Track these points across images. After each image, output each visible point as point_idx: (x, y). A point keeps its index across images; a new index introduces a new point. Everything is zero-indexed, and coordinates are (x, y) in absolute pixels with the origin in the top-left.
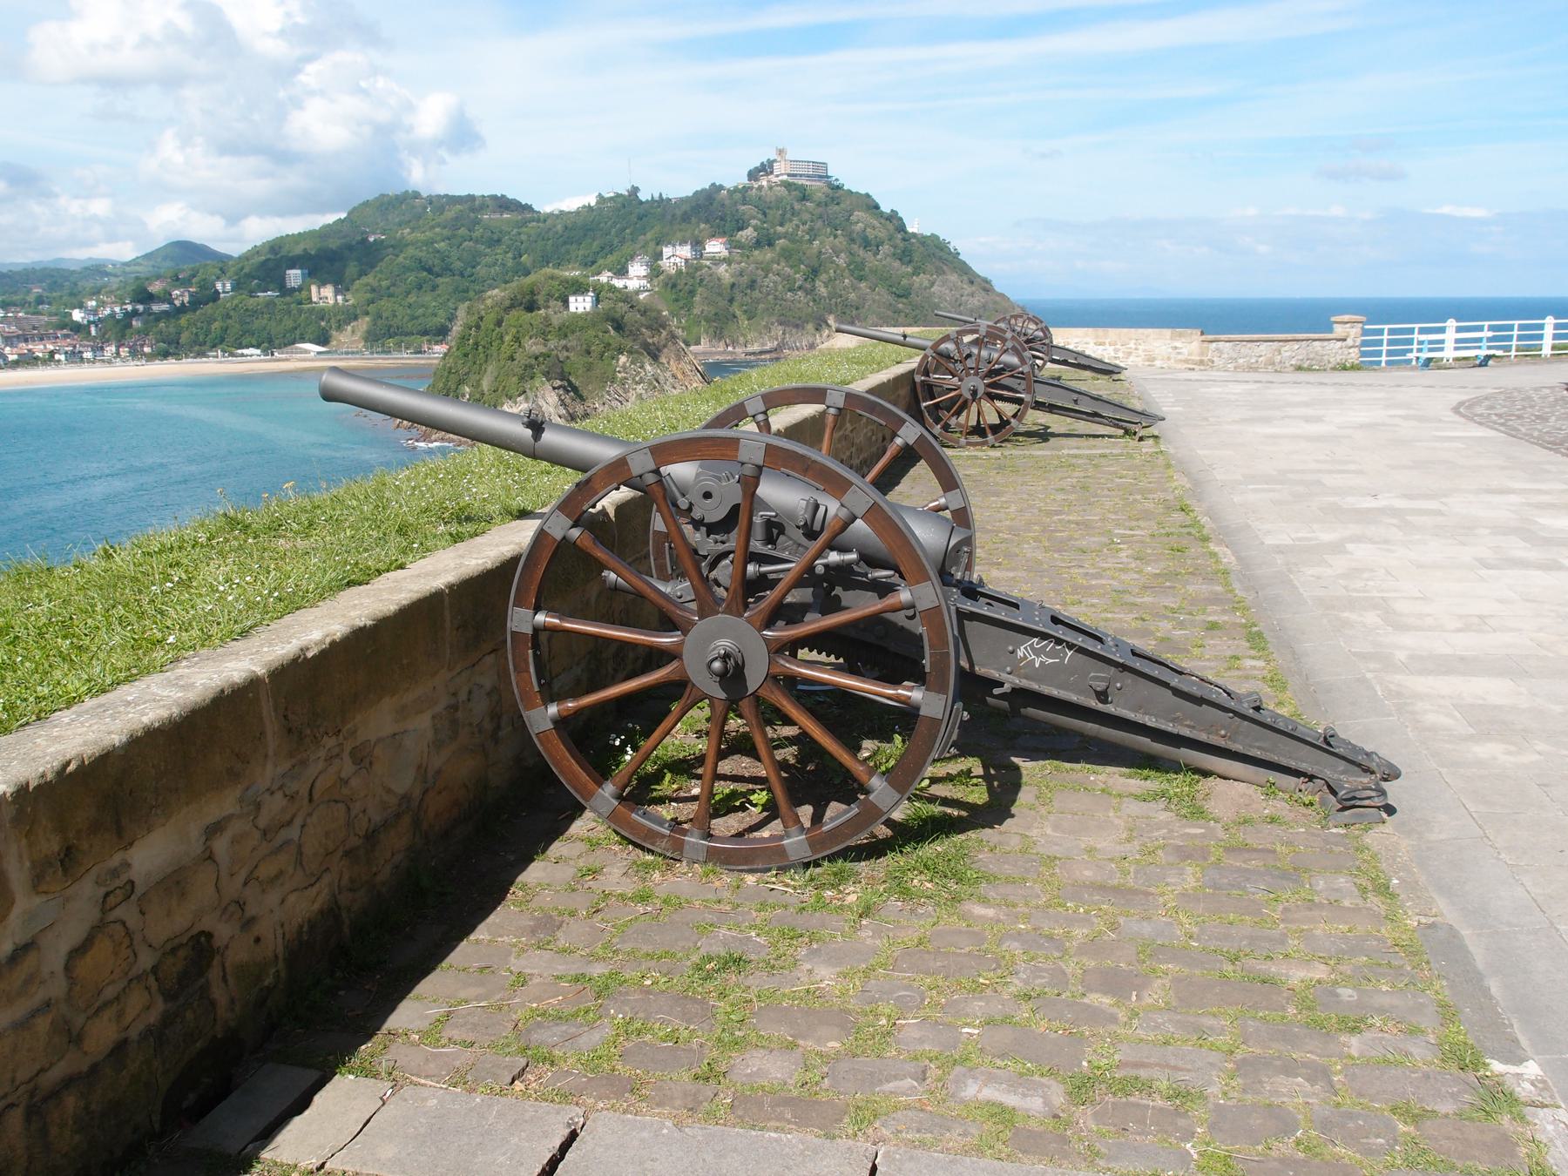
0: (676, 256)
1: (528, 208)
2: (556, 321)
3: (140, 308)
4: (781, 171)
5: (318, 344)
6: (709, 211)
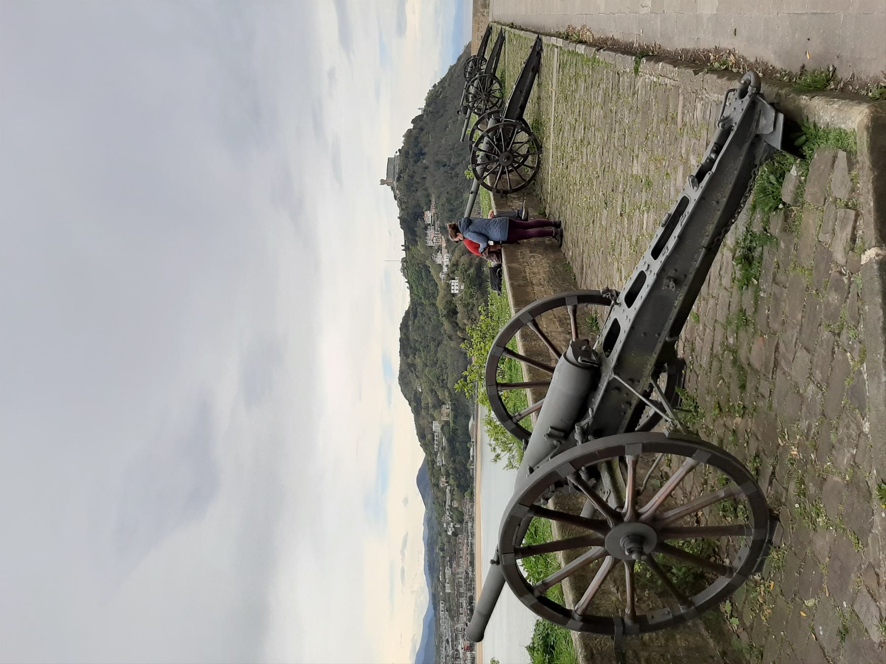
6: (411, 222)
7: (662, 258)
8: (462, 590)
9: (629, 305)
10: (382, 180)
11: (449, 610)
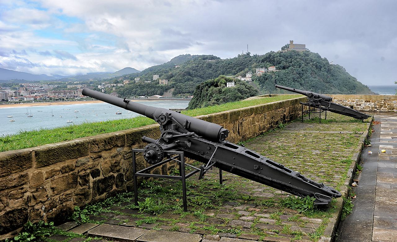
0: (260, 72)
1: (219, 58)
2: (223, 90)
3: (115, 85)
4: (291, 49)
5: (160, 95)
6: (269, 59)
7: (267, 164)
8: (68, 94)
9: (246, 152)
10: (293, 41)
11: (54, 89)
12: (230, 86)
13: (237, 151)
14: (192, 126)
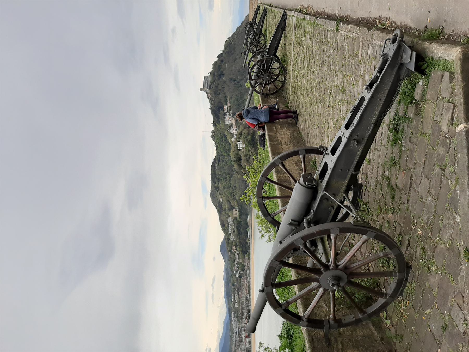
6: (217, 111)
7: (350, 129)
8: (244, 306)
12: (241, 146)
13: (331, 166)
14: (297, 219)
